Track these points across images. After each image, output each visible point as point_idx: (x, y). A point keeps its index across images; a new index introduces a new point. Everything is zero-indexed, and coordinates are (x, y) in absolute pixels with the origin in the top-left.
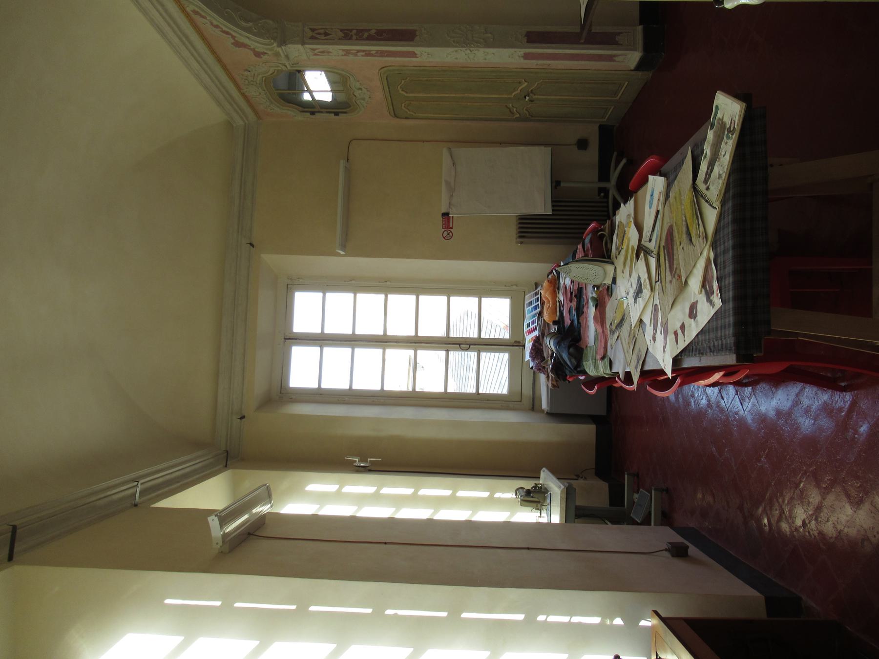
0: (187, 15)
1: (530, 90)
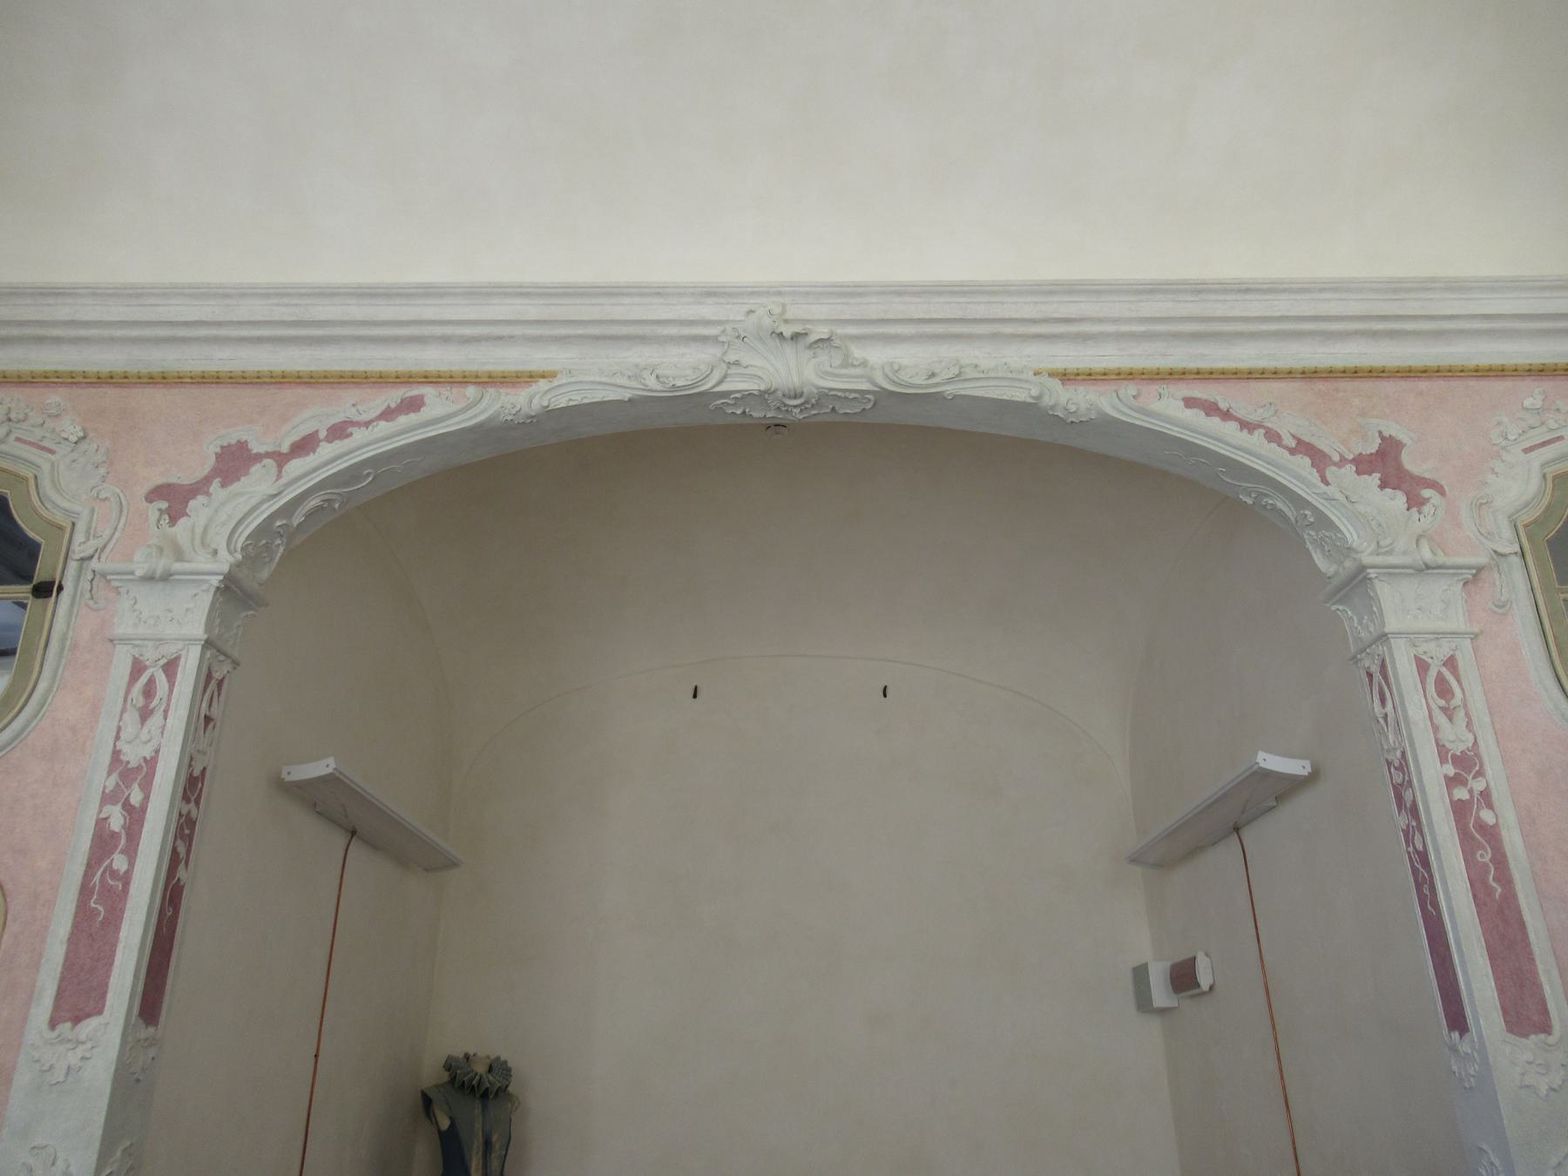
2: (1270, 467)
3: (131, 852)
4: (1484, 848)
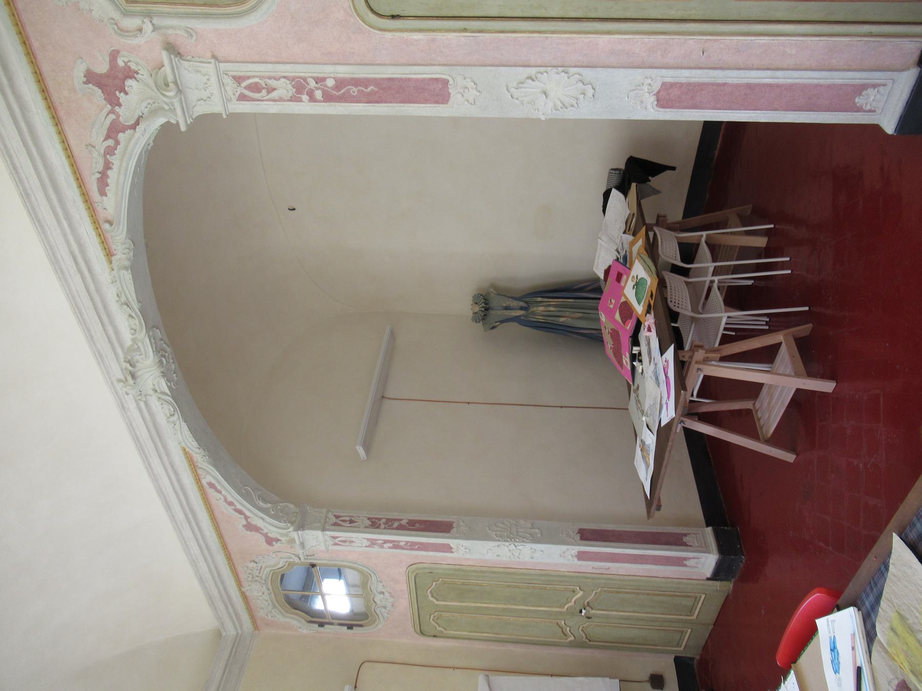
0: (201, 488)
1: (586, 602)
2: (133, 157)
3: (399, 542)
4: (349, 90)
